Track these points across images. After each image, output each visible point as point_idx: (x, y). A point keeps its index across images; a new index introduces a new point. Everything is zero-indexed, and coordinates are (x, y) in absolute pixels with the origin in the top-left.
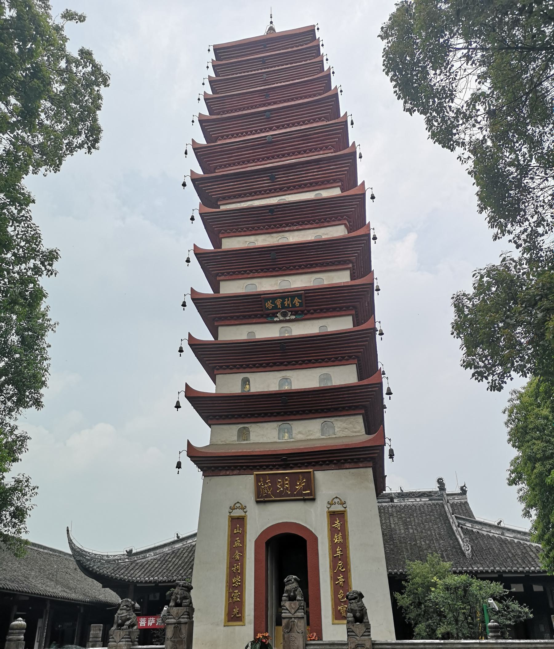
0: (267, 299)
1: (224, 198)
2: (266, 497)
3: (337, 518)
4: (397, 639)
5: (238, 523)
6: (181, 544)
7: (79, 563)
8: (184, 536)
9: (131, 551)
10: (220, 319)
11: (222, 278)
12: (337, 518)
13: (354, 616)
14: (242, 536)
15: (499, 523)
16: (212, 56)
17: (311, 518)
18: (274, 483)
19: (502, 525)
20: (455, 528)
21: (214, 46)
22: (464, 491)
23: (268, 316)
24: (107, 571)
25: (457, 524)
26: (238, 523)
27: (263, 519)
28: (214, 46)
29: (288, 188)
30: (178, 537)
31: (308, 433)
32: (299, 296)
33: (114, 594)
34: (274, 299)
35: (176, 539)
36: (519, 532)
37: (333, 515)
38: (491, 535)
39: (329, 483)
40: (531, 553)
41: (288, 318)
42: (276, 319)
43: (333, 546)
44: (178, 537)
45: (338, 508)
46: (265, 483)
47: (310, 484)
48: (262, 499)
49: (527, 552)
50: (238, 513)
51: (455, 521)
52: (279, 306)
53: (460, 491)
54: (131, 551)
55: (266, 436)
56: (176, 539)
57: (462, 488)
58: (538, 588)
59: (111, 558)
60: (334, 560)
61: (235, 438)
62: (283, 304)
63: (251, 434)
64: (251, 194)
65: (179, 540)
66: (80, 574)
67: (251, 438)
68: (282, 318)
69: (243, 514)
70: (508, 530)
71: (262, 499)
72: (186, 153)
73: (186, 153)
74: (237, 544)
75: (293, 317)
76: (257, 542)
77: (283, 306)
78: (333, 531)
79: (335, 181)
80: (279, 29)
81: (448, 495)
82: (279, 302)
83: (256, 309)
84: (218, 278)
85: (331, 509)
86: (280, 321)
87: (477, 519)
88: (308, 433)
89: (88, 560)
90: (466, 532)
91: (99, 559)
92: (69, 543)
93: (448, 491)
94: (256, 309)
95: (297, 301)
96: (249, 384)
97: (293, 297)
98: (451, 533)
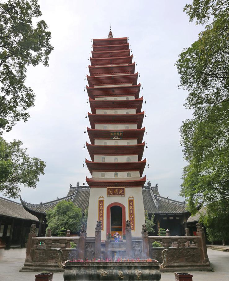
0: (112, 132)
1: (97, 96)
2: (110, 195)
3: (131, 202)
4: (122, 231)
5: (101, 202)
6: (59, 201)
7: (24, 207)
8: (60, 198)
9: (42, 203)
10: (96, 137)
11: (96, 123)
12: (131, 202)
13: (144, 230)
14: (103, 206)
15: (168, 197)
16: (92, 43)
17: (123, 201)
18: (113, 191)
19: (169, 198)
20: (153, 199)
21: (93, 40)
22: (157, 186)
23: (111, 137)
24: (34, 209)
25: (154, 197)
26: (101, 202)
27: (109, 201)
28: (93, 40)
29: (118, 95)
30: (58, 198)
31: (122, 176)
32: (122, 132)
33: (38, 219)
34: (113, 133)
35: (57, 199)
36: (174, 201)
37: (130, 201)
38: (165, 201)
39: (128, 191)
40: (177, 207)
41: (117, 139)
42: (113, 139)
43: (130, 210)
44: (58, 198)
45: (131, 199)
46: (110, 191)
47: (123, 192)
48: (109, 195)
49: (176, 207)
50: (101, 199)
51: (154, 196)
52: (115, 135)
53: (155, 186)
54: (42, 203)
55: (110, 176)
56: (57, 199)
57: (156, 185)
58: (178, 218)
59: (35, 205)
60: (130, 214)
61: (100, 176)
62: (116, 134)
63: (105, 175)
64: (106, 95)
65: (58, 200)
66: (25, 211)
67: (106, 176)
68: (115, 139)
69: (103, 199)
70: (170, 200)
71: (109, 195)
72: (85, 79)
73: (85, 79)
74: (101, 208)
75: (119, 138)
76: (107, 208)
77: (116, 135)
78: (130, 205)
79: (133, 94)
80: (115, 36)
81: (152, 187)
82: (115, 134)
83: (107, 135)
84: (95, 123)
85: (129, 199)
86: (115, 139)
87: (161, 196)
88: (122, 176)
89: (27, 206)
90: (157, 200)
91: (34, 206)
92: (21, 199)
93: (152, 186)
94: (107, 135)
95: (121, 134)
96: (105, 159)
97: (120, 132)
98: (152, 200)
